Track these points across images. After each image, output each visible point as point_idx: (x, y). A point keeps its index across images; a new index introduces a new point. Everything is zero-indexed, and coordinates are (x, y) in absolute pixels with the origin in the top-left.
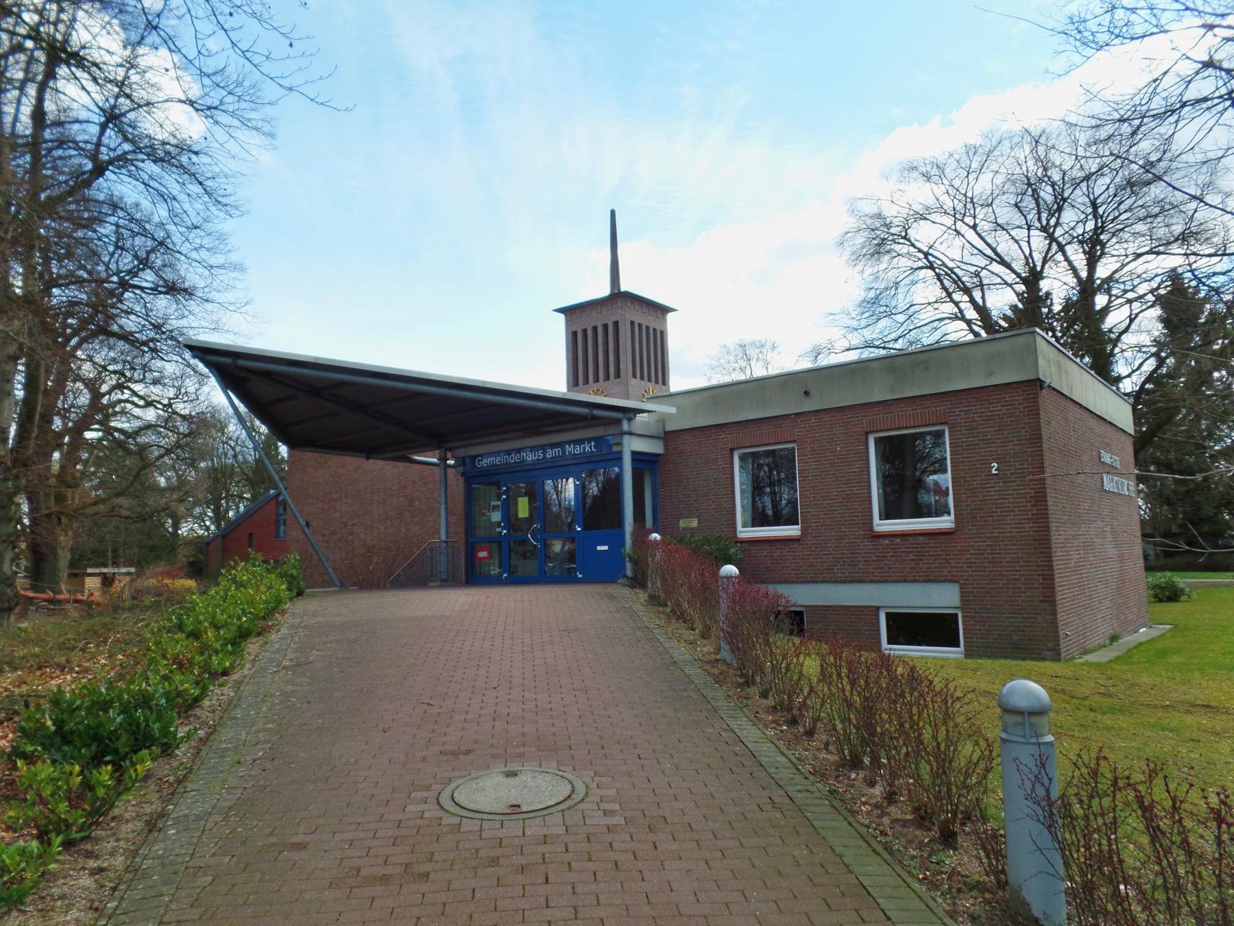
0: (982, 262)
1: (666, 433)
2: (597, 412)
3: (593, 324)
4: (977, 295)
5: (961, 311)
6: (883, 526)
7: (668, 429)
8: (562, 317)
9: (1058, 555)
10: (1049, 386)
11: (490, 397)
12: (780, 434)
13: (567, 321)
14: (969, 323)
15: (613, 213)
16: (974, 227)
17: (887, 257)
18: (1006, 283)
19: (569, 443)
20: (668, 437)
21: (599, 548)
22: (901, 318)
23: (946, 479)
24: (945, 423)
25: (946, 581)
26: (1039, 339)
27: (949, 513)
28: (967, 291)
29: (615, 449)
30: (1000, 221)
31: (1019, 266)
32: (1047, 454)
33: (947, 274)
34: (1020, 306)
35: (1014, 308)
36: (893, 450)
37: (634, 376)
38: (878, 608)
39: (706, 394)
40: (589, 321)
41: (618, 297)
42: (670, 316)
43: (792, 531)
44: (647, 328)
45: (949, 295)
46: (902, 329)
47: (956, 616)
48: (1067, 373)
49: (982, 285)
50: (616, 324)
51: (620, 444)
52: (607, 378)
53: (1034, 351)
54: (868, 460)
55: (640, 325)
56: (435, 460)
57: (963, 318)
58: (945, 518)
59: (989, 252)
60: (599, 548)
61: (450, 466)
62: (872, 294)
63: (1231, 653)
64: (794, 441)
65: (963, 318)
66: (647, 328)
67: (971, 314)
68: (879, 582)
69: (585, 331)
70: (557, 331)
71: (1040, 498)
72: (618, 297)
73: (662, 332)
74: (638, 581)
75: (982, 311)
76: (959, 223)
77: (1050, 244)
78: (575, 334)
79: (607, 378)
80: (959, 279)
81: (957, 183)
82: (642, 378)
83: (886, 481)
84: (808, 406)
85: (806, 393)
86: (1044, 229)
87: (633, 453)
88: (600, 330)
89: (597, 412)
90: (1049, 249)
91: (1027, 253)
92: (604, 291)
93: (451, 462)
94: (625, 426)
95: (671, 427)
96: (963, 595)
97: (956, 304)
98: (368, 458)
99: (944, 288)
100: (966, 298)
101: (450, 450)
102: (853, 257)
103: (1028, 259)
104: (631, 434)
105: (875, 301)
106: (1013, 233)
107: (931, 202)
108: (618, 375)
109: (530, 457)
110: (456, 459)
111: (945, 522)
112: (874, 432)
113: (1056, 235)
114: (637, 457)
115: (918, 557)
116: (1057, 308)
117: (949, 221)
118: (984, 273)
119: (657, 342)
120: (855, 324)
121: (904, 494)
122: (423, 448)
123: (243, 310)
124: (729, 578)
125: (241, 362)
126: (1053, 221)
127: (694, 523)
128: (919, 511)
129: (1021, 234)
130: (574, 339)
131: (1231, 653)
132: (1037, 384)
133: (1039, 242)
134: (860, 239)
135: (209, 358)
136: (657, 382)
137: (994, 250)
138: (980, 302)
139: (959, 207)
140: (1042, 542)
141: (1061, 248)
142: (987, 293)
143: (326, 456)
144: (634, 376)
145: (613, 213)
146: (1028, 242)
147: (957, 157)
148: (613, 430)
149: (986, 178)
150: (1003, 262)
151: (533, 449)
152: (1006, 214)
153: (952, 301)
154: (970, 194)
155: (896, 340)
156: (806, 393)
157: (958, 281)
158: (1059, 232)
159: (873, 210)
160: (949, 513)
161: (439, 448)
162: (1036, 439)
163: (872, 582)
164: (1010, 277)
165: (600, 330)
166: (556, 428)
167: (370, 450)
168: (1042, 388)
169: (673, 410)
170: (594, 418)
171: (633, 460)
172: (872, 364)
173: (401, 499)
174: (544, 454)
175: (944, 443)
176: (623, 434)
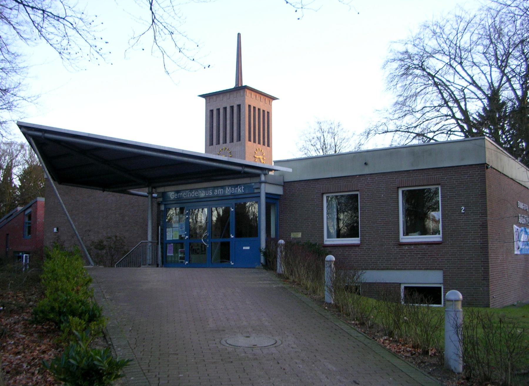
0: (465, 84)
1: (284, 182)
2: (247, 170)
3: (224, 106)
4: (462, 104)
5: (453, 114)
6: (404, 239)
7: (286, 180)
8: (203, 100)
9: (492, 255)
10: (491, 167)
11: (165, 155)
12: (351, 187)
13: (206, 103)
14: (457, 119)
15: (239, 35)
16: (461, 64)
17: (410, 77)
18: (478, 98)
19: (229, 186)
20: (286, 185)
21: (244, 248)
22: (418, 115)
23: (437, 215)
24: (439, 184)
25: (436, 269)
26: (486, 142)
27: (439, 234)
28: (456, 101)
29: (256, 191)
30: (475, 61)
31: (485, 88)
32: (488, 203)
33: (445, 89)
34: (488, 109)
35: (484, 109)
36: (410, 196)
37: (250, 140)
38: (400, 284)
39: (309, 161)
40: (222, 103)
41: (240, 89)
42: (274, 102)
43: (355, 241)
44: (259, 109)
45: (446, 102)
46: (418, 122)
47: (440, 288)
48: (501, 160)
49: (465, 98)
50: (239, 106)
51: (259, 188)
52: (232, 141)
53: (483, 147)
54: (398, 202)
55: (254, 108)
56: (146, 194)
57: (454, 117)
58: (437, 236)
59: (468, 79)
60: (244, 248)
61: (154, 198)
62: (401, 99)
63: (1, 5)
64: (358, 191)
65: (454, 117)
66: (259, 109)
67: (459, 115)
68: (402, 269)
69: (218, 110)
70: (200, 108)
71: (484, 226)
72: (240, 89)
73: (268, 113)
74: (269, 265)
75: (464, 112)
76: (452, 61)
77: (502, 77)
78: (212, 111)
79: (232, 141)
80: (453, 93)
81: (451, 37)
82: (255, 142)
83: (408, 213)
84: (367, 171)
85: (366, 164)
86: (499, 67)
87: (267, 194)
88: (228, 110)
89: (247, 170)
90: (501, 80)
91: (490, 82)
92: (232, 85)
93: (155, 195)
94: (263, 178)
95: (288, 179)
96: (444, 276)
97: (450, 108)
98: (104, 191)
99: (443, 98)
100: (456, 105)
101: (155, 188)
102: (391, 76)
103: (491, 84)
104: (265, 182)
105: (404, 104)
106: (482, 68)
107: (437, 47)
108: (239, 139)
109: (202, 194)
110: (158, 193)
111: (437, 238)
112: (402, 187)
113: (506, 71)
114: (269, 196)
115: (423, 257)
116: (508, 110)
117: (446, 59)
118: (466, 91)
119: (265, 118)
120: (391, 117)
121: (417, 222)
122: (138, 186)
123: (36, 101)
124: (331, 261)
125: (47, 135)
126: (504, 64)
127: (299, 235)
128: (424, 231)
129: (487, 69)
130: (211, 114)
131: (1, 5)
132: (484, 166)
133: (496, 74)
134: (396, 65)
135: (30, 132)
136: (264, 144)
137: (472, 78)
138: (463, 107)
139: (453, 51)
140: (484, 248)
141: (509, 80)
142: (468, 104)
143: (71, 187)
144: (250, 140)
145: (239, 35)
146: (491, 75)
147: (451, 22)
148: (256, 180)
149: (467, 36)
150: (477, 86)
151: (206, 189)
152: (479, 58)
153: (448, 106)
154: (458, 45)
155: (415, 127)
156: (366, 164)
157: (451, 94)
158: (507, 70)
159: (403, 49)
160: (439, 234)
161: (148, 186)
162: (483, 195)
163: (397, 269)
164: (481, 95)
165: (228, 110)
166: (221, 177)
167: (105, 185)
168: (487, 168)
169: (290, 170)
170: (245, 173)
171: (266, 198)
172: (402, 149)
173: (117, 215)
174: (213, 192)
175: (438, 196)
176: (261, 183)
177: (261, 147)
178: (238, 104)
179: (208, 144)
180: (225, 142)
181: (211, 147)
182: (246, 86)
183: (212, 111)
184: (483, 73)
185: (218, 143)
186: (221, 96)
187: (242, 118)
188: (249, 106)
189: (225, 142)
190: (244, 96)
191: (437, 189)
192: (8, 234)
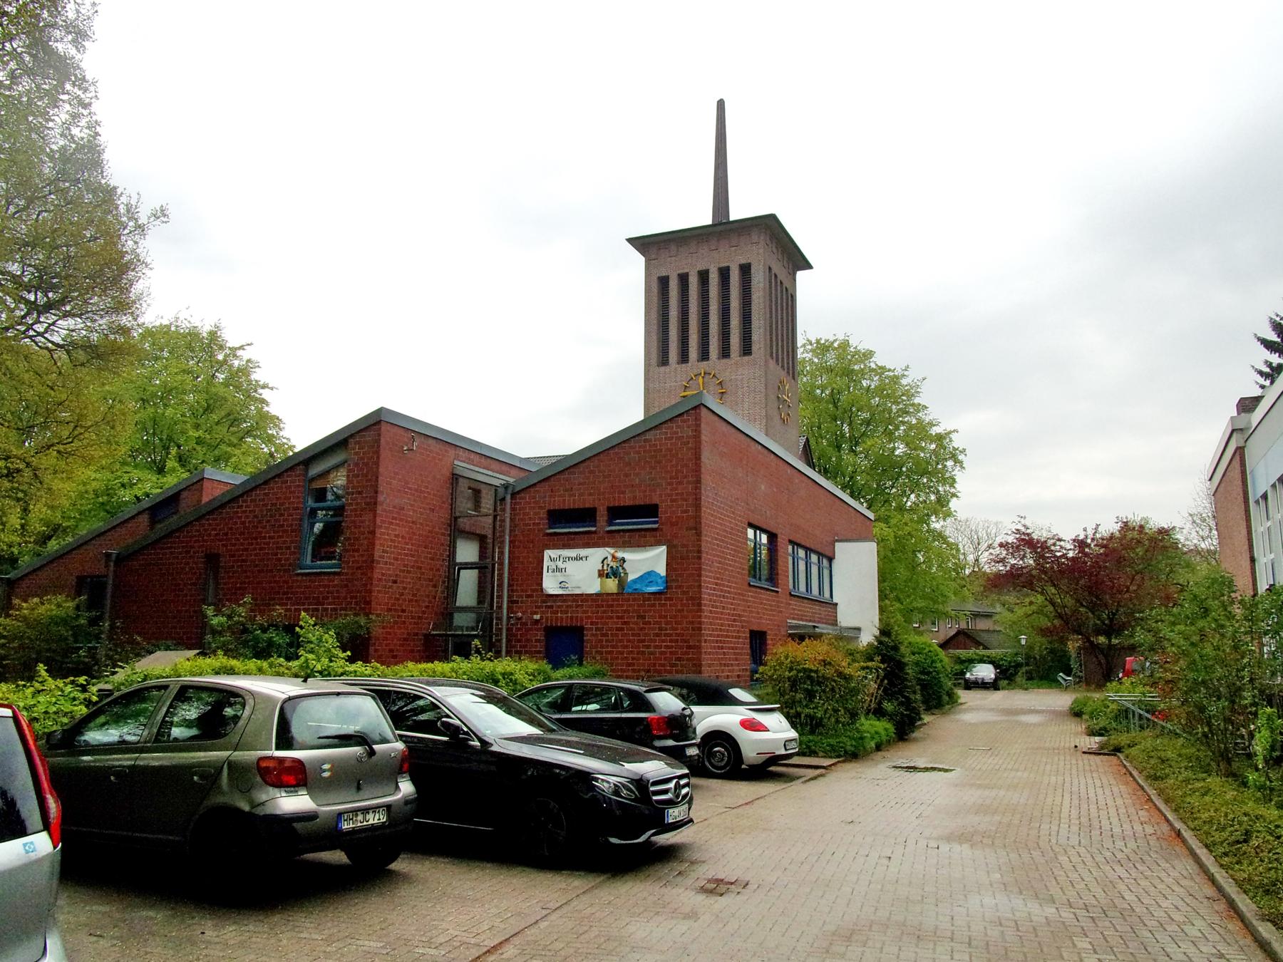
40: (692, 263)
52: (725, 353)
78: (664, 282)
79: (725, 353)
130: (659, 289)
178: (743, 262)
179: (654, 361)
180: (704, 355)
185: (684, 358)
189: (704, 355)
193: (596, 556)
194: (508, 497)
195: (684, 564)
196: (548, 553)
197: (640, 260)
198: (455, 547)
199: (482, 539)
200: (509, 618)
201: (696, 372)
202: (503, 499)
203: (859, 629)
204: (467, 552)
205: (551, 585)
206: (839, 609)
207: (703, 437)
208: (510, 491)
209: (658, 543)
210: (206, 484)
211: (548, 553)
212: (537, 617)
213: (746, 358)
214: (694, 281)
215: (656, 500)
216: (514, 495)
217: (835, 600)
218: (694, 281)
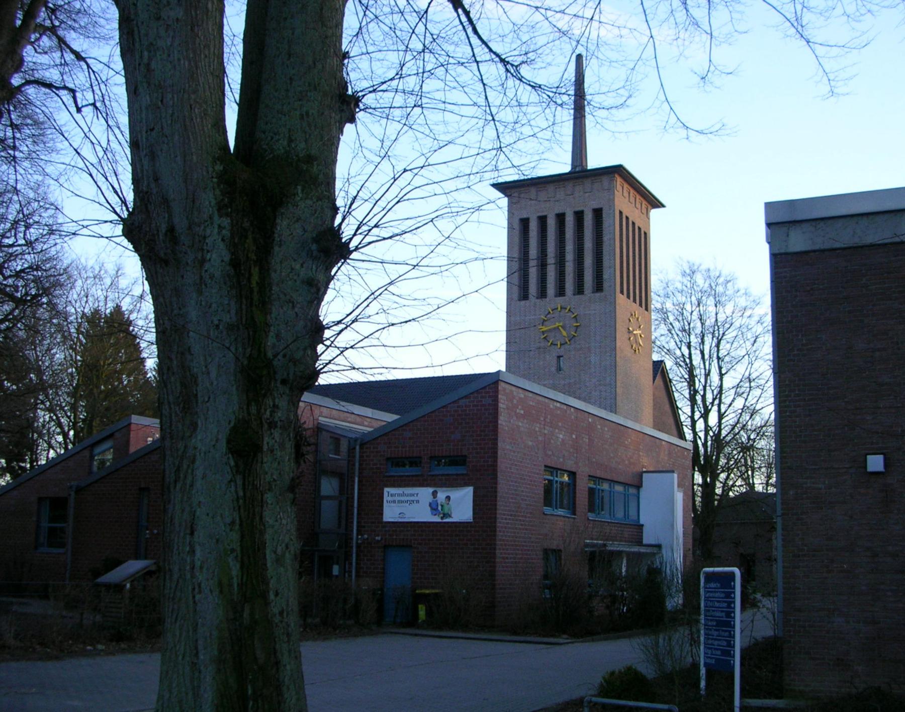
40: (550, 205)
42: (654, 213)
50: (598, 213)
52: (579, 289)
73: (645, 234)
78: (525, 223)
79: (579, 289)
108: (599, 286)
130: (520, 230)
144: (622, 292)
177: (636, 306)
178: (596, 207)
179: (516, 296)
180: (561, 292)
181: (523, 302)
182: (618, 171)
183: (525, 223)
184: (391, 283)
185: (542, 294)
186: (551, 188)
187: (605, 238)
188: (621, 213)
189: (561, 292)
190: (611, 190)
191: (710, 577)
192: (559, 357)
193: (424, 493)
194: (358, 447)
195: (485, 504)
196: (386, 490)
197: (504, 202)
198: (320, 483)
199: (340, 476)
200: (357, 539)
201: (553, 306)
202: (354, 448)
203: (659, 546)
204: (329, 486)
205: (391, 513)
206: (644, 528)
207: (501, 405)
208: (359, 442)
209: (466, 485)
210: (132, 426)
211: (386, 490)
212: (378, 538)
213: (598, 295)
214: (551, 223)
215: (465, 453)
216: (362, 446)
217: (641, 522)
218: (551, 223)
